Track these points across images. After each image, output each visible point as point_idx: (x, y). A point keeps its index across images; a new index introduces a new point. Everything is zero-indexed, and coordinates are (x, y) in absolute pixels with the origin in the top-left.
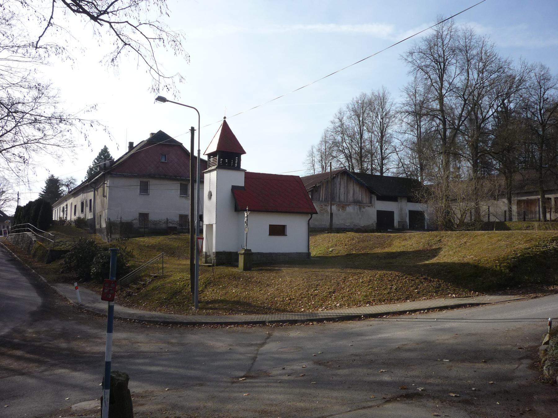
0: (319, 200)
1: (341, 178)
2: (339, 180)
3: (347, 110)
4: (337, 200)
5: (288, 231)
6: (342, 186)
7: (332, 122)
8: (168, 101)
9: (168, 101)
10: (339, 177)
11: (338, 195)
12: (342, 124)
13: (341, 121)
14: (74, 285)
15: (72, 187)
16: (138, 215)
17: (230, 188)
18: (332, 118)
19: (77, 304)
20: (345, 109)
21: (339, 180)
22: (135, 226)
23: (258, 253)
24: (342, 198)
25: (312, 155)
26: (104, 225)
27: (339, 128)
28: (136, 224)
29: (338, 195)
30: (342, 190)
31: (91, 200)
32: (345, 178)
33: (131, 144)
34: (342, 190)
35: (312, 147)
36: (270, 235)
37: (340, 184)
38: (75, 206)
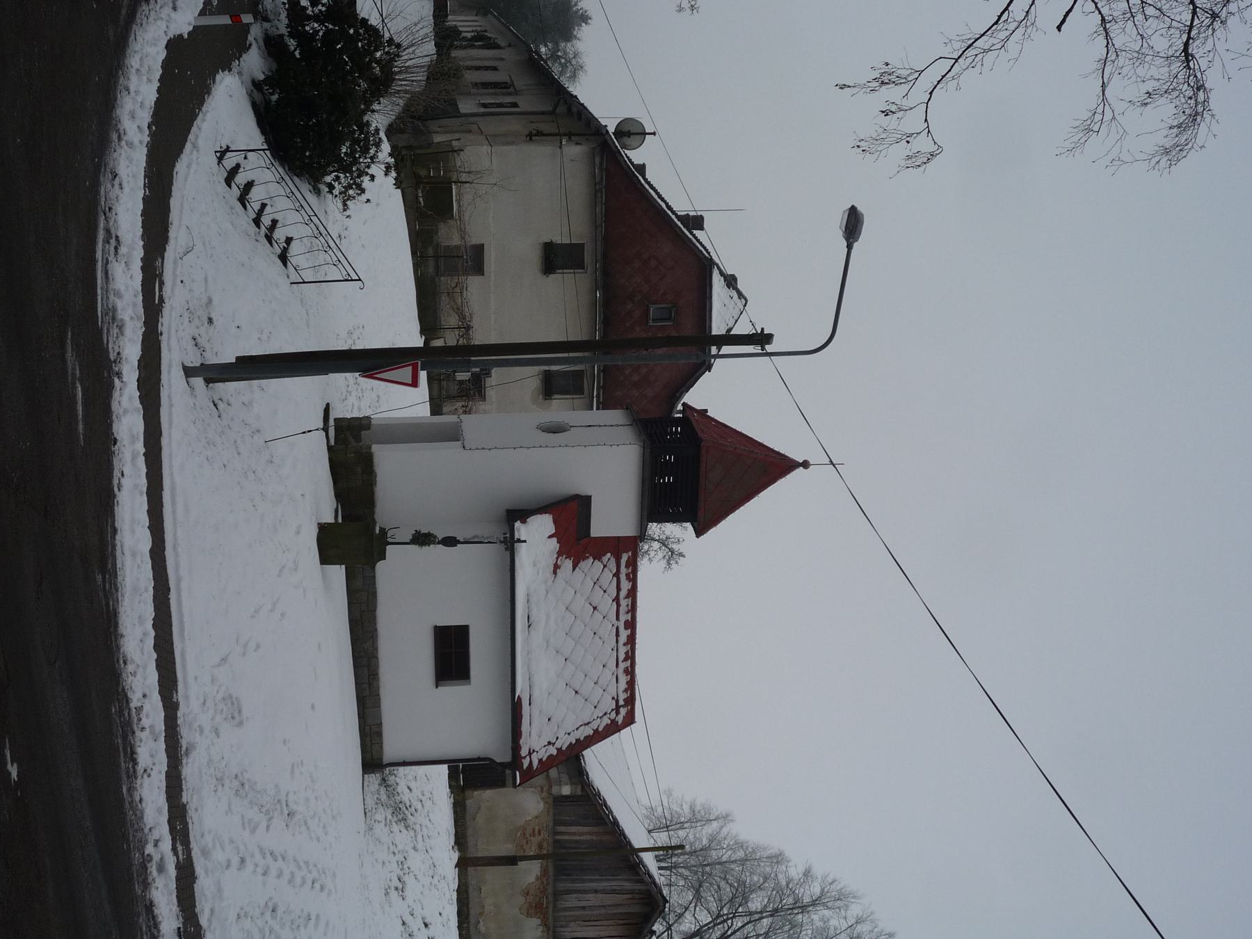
0: (557, 822)
1: (631, 892)
2: (628, 885)
3: (851, 921)
4: (562, 886)
5: (453, 692)
6: (610, 899)
7: (807, 873)
8: (850, 247)
9: (850, 247)
10: (638, 887)
11: (578, 886)
12: (804, 909)
13: (814, 903)
14: (248, 25)
15: (556, 69)
16: (475, 241)
17: (584, 491)
18: (818, 871)
19: (141, 800)
20: (855, 910)
21: (628, 885)
22: (441, 226)
23: (374, 594)
24: (571, 901)
25: (697, 818)
26: (438, 139)
27: (791, 900)
28: (448, 236)
29: (578, 886)
30: (592, 900)
31: (515, 105)
32: (635, 909)
33: (696, 222)
34: (592, 900)
35: (726, 818)
36: (436, 627)
37: (613, 892)
38: (495, 69)
